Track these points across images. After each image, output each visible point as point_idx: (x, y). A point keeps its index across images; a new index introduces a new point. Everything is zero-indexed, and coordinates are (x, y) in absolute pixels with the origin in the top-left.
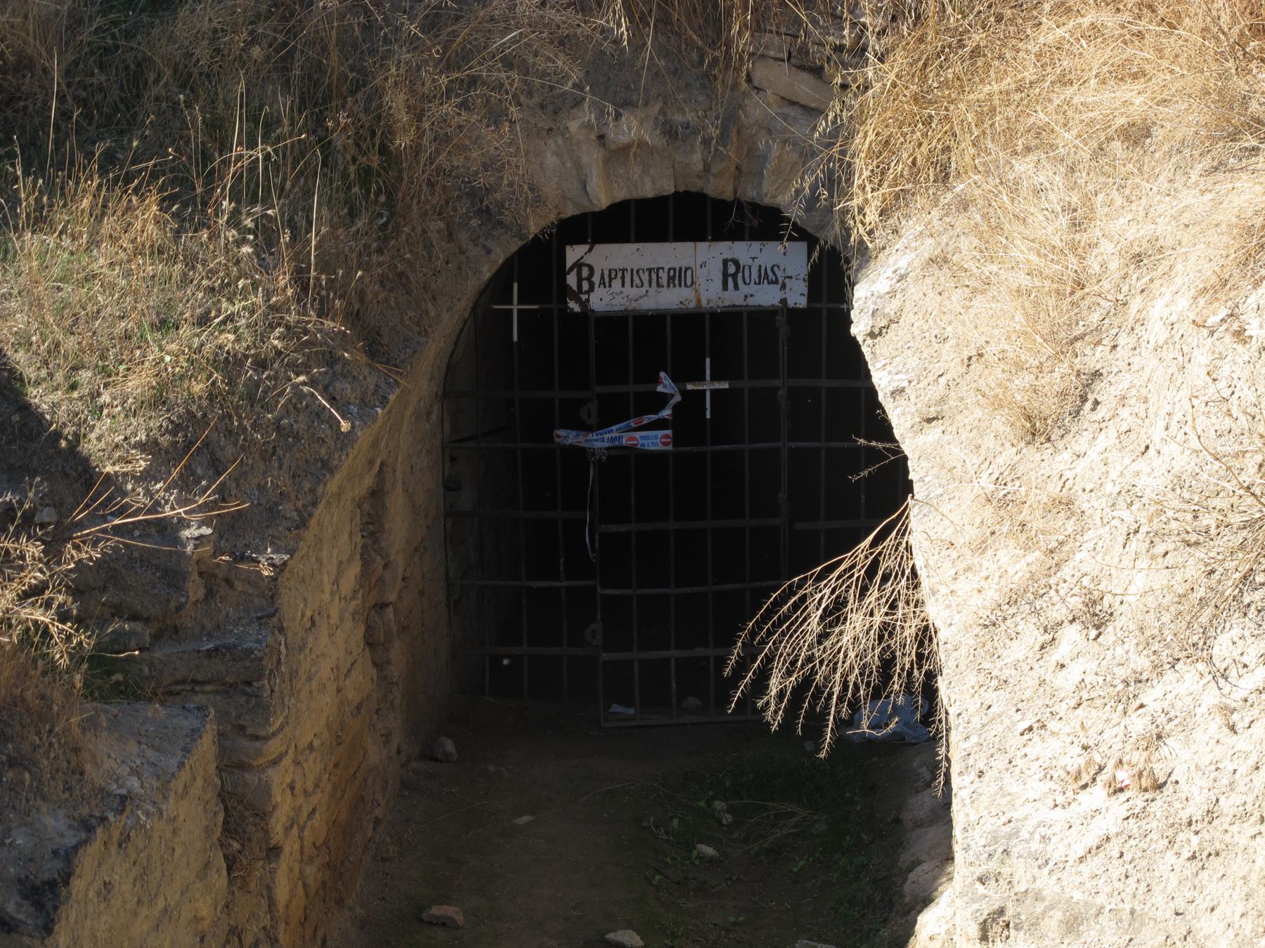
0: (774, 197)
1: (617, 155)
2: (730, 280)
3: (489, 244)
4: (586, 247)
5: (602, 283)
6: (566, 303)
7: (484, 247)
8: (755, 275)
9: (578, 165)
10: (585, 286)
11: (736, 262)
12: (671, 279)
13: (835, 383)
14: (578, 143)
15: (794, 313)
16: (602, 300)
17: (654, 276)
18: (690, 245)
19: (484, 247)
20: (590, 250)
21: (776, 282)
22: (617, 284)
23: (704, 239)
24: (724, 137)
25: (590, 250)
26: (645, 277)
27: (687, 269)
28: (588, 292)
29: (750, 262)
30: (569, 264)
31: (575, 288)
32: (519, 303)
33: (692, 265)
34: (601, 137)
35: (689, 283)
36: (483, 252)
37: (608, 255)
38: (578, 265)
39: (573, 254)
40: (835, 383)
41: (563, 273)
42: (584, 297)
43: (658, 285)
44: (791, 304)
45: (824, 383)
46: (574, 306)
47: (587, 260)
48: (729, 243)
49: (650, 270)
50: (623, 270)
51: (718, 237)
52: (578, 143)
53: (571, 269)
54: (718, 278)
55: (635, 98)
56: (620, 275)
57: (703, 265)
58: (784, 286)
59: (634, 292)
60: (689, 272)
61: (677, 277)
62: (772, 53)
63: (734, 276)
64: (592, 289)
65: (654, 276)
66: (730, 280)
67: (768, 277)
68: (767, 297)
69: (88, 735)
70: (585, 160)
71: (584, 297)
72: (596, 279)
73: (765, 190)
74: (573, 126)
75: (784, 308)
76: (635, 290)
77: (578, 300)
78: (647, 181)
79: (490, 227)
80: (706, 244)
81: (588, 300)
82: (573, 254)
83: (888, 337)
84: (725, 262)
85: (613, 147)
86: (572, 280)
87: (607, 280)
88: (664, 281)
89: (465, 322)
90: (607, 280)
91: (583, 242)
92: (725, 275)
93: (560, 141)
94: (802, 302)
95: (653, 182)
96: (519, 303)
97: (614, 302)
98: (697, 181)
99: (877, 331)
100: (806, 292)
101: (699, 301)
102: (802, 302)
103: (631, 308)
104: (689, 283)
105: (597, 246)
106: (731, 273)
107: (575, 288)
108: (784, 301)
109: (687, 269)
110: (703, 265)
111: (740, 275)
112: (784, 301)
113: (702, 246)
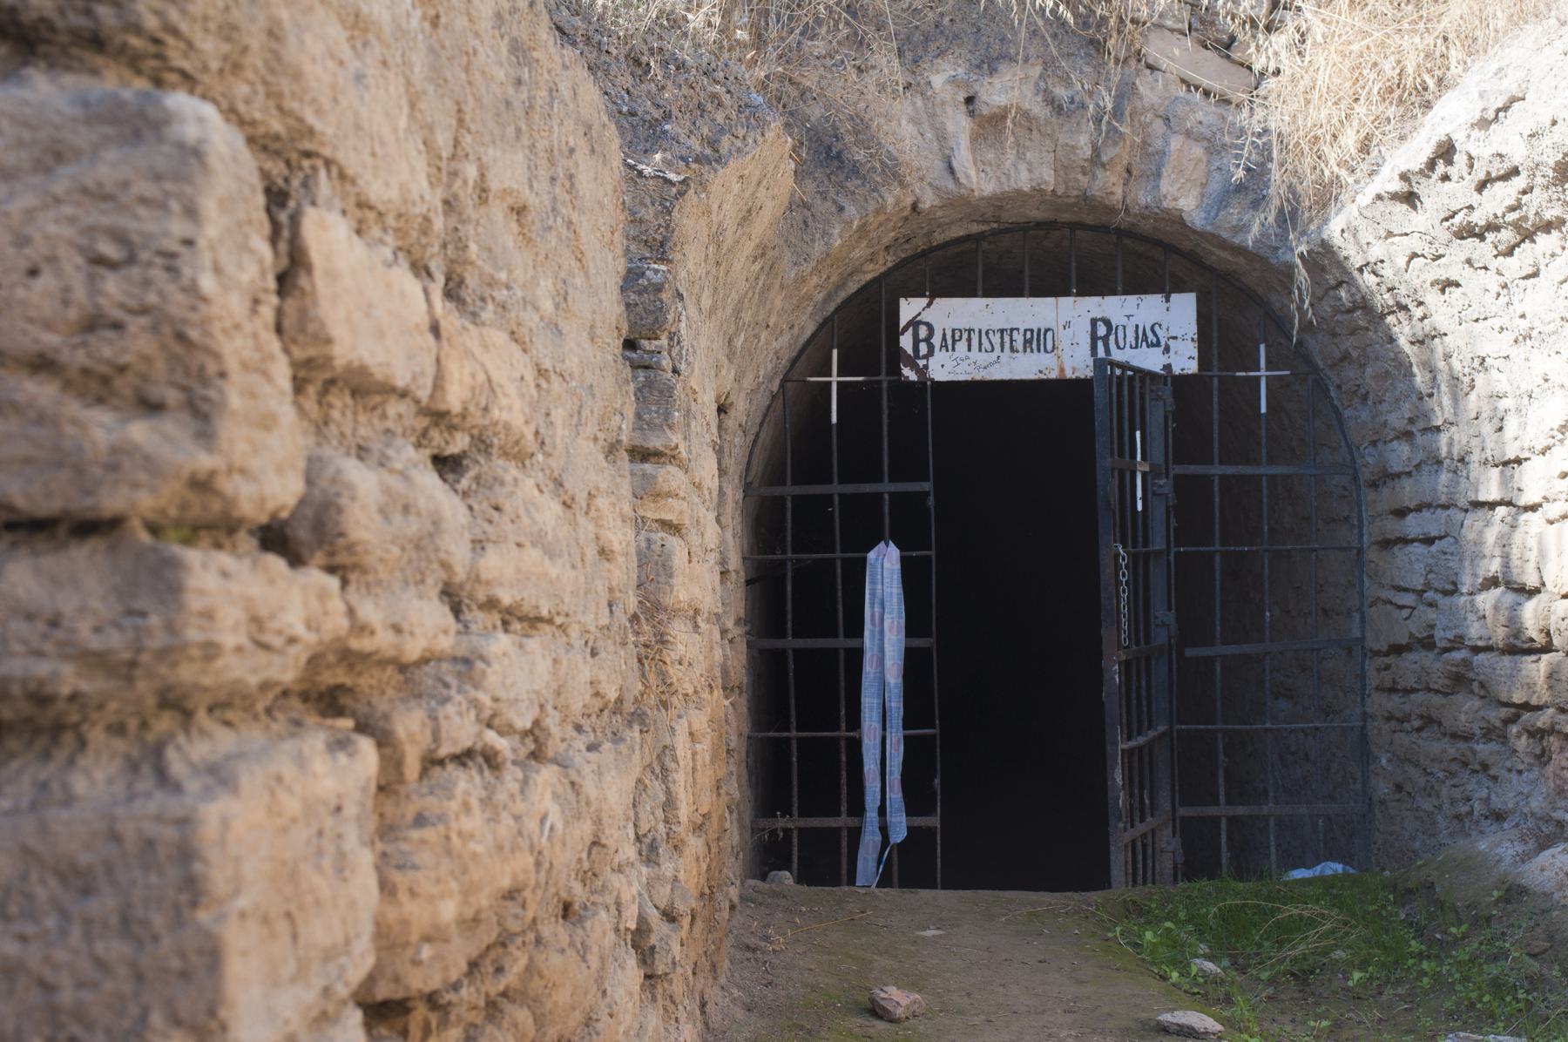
0: (1176, 199)
1: (989, 126)
2: (1100, 344)
3: (841, 200)
4: (925, 301)
5: (944, 345)
6: (899, 373)
7: (835, 202)
8: (1131, 338)
9: (942, 137)
10: (923, 349)
11: (1107, 323)
12: (1027, 342)
13: (1230, 470)
14: (943, 103)
15: (1182, 381)
16: (944, 368)
17: (1007, 339)
18: (1052, 300)
19: (835, 202)
20: (929, 305)
21: (1158, 344)
22: (962, 346)
23: (1067, 294)
24: (1117, 113)
25: (929, 305)
26: (996, 339)
27: (1047, 331)
28: (926, 357)
29: (1124, 321)
30: (902, 323)
31: (910, 351)
32: (830, 383)
33: (1053, 326)
34: (970, 100)
35: (1049, 348)
36: (833, 209)
37: (949, 313)
38: (914, 324)
39: (909, 308)
40: (1230, 470)
41: (894, 333)
42: (921, 363)
43: (1013, 350)
44: (1177, 370)
45: (1217, 470)
46: (909, 374)
47: (925, 317)
48: (1099, 299)
49: (1002, 331)
50: (970, 331)
51: (1082, 293)
52: (943, 103)
53: (906, 329)
54: (1086, 341)
55: (1012, 51)
56: (965, 336)
57: (1067, 325)
58: (1167, 350)
59: (983, 358)
60: (1049, 334)
61: (1036, 340)
62: (1169, 23)
63: (1105, 339)
64: (931, 352)
65: (1007, 339)
66: (1100, 344)
67: (1146, 338)
68: (1151, 361)
69: (420, 209)
70: (950, 128)
71: (921, 363)
72: (937, 341)
73: (1164, 190)
74: (938, 81)
75: (1168, 378)
76: (983, 354)
77: (914, 367)
78: (1023, 167)
79: (842, 177)
80: (1071, 299)
81: (926, 367)
82: (909, 308)
83: (1507, 122)
84: (1094, 322)
85: (985, 111)
86: (906, 342)
87: (950, 342)
88: (1019, 344)
89: (774, 397)
90: (950, 342)
91: (923, 296)
92: (1094, 338)
93: (919, 103)
94: (1192, 367)
95: (1030, 171)
96: (830, 383)
97: (958, 369)
98: (1080, 177)
99: (1491, 115)
100: (1195, 354)
101: (1062, 370)
102: (1192, 367)
103: (978, 378)
104: (1049, 348)
105: (937, 300)
106: (1101, 332)
107: (910, 351)
108: (1168, 367)
109: (1047, 331)
110: (1067, 325)
111: (1112, 338)
112: (1168, 367)
113: (1066, 302)
